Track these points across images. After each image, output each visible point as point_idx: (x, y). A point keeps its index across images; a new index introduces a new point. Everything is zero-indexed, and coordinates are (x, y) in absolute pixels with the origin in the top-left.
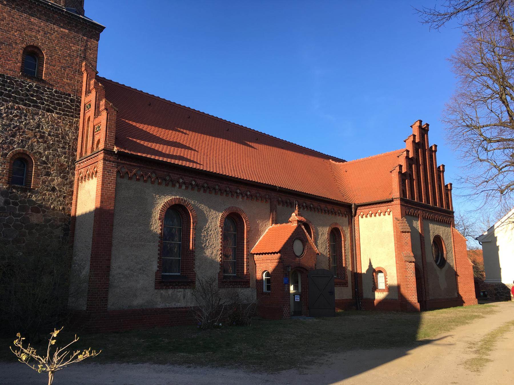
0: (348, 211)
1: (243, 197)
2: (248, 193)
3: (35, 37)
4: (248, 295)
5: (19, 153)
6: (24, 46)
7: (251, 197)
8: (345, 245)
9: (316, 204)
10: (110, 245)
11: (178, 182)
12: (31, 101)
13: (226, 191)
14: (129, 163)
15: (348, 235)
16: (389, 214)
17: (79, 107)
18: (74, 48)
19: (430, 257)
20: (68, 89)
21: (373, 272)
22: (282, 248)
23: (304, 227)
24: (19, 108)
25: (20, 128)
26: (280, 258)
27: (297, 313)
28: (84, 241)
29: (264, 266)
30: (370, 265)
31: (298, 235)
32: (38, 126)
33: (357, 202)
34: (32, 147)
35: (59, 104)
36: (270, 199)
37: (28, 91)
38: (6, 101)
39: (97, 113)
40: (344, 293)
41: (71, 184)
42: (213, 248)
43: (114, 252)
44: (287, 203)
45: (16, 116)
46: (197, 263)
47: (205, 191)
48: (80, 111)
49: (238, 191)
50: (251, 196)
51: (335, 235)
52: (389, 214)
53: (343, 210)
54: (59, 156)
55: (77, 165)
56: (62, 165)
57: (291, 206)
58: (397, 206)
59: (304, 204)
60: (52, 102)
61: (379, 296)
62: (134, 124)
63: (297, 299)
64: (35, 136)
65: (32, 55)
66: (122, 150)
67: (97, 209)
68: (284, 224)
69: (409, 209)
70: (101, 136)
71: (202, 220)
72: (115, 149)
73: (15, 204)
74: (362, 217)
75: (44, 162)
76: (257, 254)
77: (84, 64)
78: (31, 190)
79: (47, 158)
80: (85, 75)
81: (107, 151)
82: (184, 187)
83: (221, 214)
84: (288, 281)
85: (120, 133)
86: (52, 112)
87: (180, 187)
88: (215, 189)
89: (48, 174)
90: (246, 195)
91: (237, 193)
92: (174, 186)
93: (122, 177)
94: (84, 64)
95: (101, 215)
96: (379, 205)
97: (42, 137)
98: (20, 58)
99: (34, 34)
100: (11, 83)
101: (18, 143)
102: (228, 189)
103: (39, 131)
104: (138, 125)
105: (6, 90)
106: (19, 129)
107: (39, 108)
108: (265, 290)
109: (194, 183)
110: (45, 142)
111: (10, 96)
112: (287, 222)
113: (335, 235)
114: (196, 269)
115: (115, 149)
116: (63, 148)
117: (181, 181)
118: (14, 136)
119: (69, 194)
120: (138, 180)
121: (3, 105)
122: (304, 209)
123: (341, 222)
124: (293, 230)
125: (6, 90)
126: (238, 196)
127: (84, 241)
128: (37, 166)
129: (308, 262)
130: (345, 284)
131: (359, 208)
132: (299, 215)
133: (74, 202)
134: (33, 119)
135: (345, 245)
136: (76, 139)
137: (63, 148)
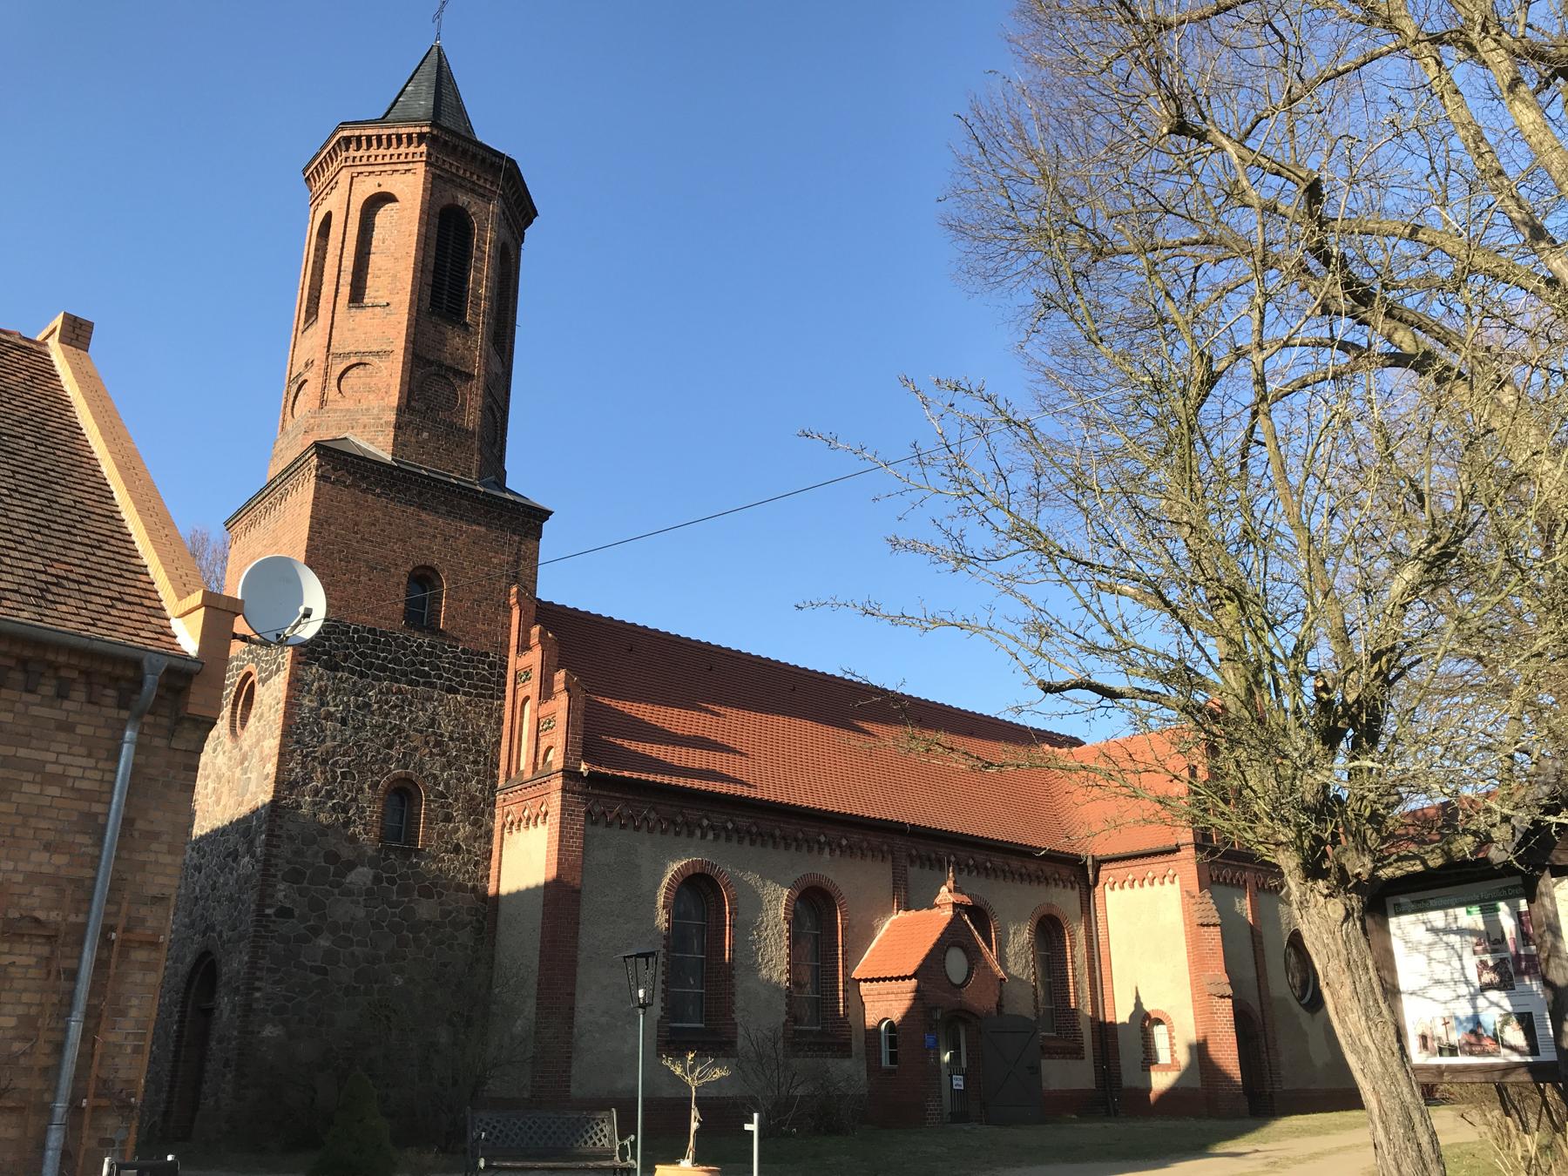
0: (1079, 874)
1: (832, 851)
2: (844, 842)
3: (429, 548)
4: (849, 1072)
5: (398, 779)
6: (409, 568)
7: (850, 851)
8: (1073, 957)
9: (998, 860)
10: (573, 962)
11: (700, 826)
12: (420, 673)
13: (796, 840)
14: (606, 795)
15: (1081, 932)
16: (1172, 882)
17: (503, 676)
18: (495, 561)
19: (1281, 985)
20: (484, 644)
21: (1144, 1021)
22: (920, 966)
23: (975, 914)
24: (400, 691)
25: (401, 730)
26: (917, 990)
27: (959, 1117)
28: (521, 948)
29: (885, 1005)
30: (1138, 1004)
31: (953, 937)
32: (433, 722)
33: (1101, 852)
34: (420, 767)
35: (468, 676)
36: (892, 853)
37: (416, 655)
38: (379, 679)
39: (546, 693)
40: (1068, 1075)
41: (489, 835)
42: (774, 960)
43: (581, 978)
44: (929, 859)
45: (396, 706)
46: (740, 1001)
47: (753, 843)
48: (505, 684)
49: (822, 839)
50: (850, 847)
51: (1050, 932)
52: (1172, 882)
53: (1065, 872)
54: (467, 780)
55: (500, 797)
56: (473, 798)
57: (939, 865)
58: (1187, 862)
59: (971, 862)
60: (457, 673)
61: (1161, 1081)
62: (606, 701)
63: (958, 1082)
64: (427, 743)
65: (424, 579)
66: (596, 768)
67: (547, 884)
68: (924, 911)
69: (1221, 870)
70: (557, 739)
71: (758, 905)
72: (584, 767)
73: (392, 881)
74: (1112, 889)
75: (442, 795)
76: (866, 980)
77: (514, 589)
78: (418, 853)
79: (447, 785)
80: (516, 613)
81: (569, 774)
82: (710, 836)
83: (786, 892)
84: (937, 1041)
85: (592, 732)
86: (456, 692)
87: (704, 836)
88: (772, 836)
89: (448, 818)
90: (840, 845)
91: (819, 842)
92: (691, 834)
93: (594, 823)
94: (514, 589)
95: (558, 895)
96: (1148, 860)
97: (438, 744)
98: (402, 592)
99: (426, 543)
100: (387, 643)
101: (398, 761)
102: (800, 835)
103: (434, 733)
104: (613, 703)
105: (378, 658)
106: (400, 732)
107: (432, 685)
108: (885, 1062)
109: (730, 826)
110: (443, 754)
111: (384, 669)
112: (931, 906)
113: (1050, 932)
114: (738, 1017)
115: (584, 767)
116: (476, 762)
117: (705, 822)
118: (390, 746)
119: (482, 853)
120: (623, 827)
121: (373, 687)
122: (970, 873)
123: (1064, 900)
124: (944, 925)
125: (378, 658)
126: (821, 850)
127: (521, 948)
128: (429, 802)
129: (980, 999)
130: (1076, 1053)
131: (1104, 867)
132: (956, 890)
133: (493, 872)
134: (424, 709)
135: (1073, 957)
136: (498, 743)
137: (476, 762)
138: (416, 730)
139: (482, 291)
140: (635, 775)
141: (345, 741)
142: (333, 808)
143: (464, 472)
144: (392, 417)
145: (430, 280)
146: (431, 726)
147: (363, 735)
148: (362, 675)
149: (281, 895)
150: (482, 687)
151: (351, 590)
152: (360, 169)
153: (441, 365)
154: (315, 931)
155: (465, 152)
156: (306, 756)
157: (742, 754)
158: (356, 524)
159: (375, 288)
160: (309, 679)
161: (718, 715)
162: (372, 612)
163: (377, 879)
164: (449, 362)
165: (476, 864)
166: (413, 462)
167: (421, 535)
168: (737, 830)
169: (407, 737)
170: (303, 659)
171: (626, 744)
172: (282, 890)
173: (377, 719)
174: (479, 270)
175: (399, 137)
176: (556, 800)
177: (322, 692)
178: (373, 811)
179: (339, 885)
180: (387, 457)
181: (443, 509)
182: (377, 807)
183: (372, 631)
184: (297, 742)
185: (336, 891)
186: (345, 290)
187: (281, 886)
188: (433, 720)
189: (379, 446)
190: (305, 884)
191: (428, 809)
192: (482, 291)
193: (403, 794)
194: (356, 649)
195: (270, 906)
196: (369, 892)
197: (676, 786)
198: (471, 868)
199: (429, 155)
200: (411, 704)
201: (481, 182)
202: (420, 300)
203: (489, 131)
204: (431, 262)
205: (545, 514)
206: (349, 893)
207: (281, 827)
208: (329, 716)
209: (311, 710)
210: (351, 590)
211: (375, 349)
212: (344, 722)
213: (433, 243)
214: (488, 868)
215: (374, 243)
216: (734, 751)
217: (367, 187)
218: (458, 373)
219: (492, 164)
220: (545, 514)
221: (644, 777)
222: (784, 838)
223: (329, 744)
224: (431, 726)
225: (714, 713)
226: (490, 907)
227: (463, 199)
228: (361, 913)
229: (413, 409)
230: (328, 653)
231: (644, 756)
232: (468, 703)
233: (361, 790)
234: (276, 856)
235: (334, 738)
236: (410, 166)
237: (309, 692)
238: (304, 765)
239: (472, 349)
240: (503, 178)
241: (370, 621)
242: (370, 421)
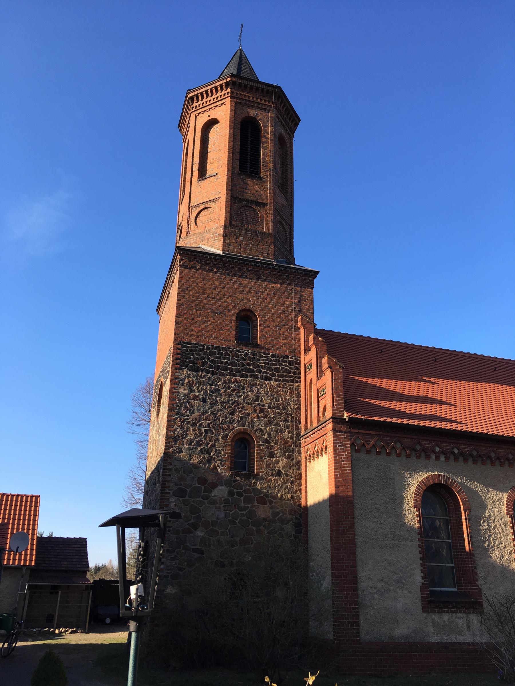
3: (247, 299)
5: (239, 433)
6: (237, 311)
11: (434, 451)
12: (247, 370)
14: (368, 433)
17: (298, 369)
18: (287, 303)
20: (285, 351)
25: (238, 404)
32: (257, 398)
35: (277, 370)
37: (244, 360)
38: (223, 375)
39: (320, 374)
41: (298, 464)
45: (234, 390)
46: (481, 573)
48: (300, 373)
54: (282, 431)
56: (286, 442)
60: (270, 369)
64: (255, 410)
65: (246, 318)
66: (354, 416)
70: (327, 401)
72: (346, 416)
73: (240, 495)
78: (255, 477)
79: (269, 435)
80: (302, 331)
81: (337, 420)
82: (443, 458)
83: (506, 496)
85: (349, 395)
88: (490, 457)
89: (272, 455)
92: (428, 457)
93: (358, 451)
97: (262, 411)
98: (233, 325)
100: (227, 354)
103: (259, 404)
105: (222, 363)
107: (256, 377)
109: (456, 451)
110: (265, 416)
111: (226, 369)
114: (480, 583)
116: (286, 421)
117: (437, 449)
118: (233, 413)
119: (297, 479)
120: (379, 453)
121: (220, 380)
125: (222, 363)
133: (303, 487)
136: (299, 408)
137: (286, 421)
138: (247, 403)
139: (268, 159)
140: (382, 419)
141: (206, 412)
142: (201, 451)
143: (266, 254)
144: (221, 231)
145: (238, 157)
146: (257, 400)
147: (216, 407)
148: (213, 373)
149: (172, 505)
150: (286, 376)
151: (203, 326)
152: (199, 111)
153: (247, 201)
154: (195, 527)
155: (251, 88)
156: (183, 422)
157: (451, 404)
158: (204, 290)
159: (210, 170)
160: (182, 377)
161: (434, 383)
162: (216, 337)
163: (231, 493)
164: (252, 198)
165: (292, 483)
166: (235, 253)
167: (242, 292)
168: (462, 454)
169: (243, 407)
170: (178, 366)
171: (378, 402)
173: (224, 398)
174: (265, 148)
176: (330, 437)
177: (190, 384)
178: (226, 453)
179: (207, 497)
180: (220, 252)
181: (254, 276)
182: (228, 450)
183: (217, 348)
184: (178, 414)
185: (206, 501)
186: (196, 173)
187: (172, 499)
188: (258, 397)
189: (215, 247)
190: (187, 498)
191: (259, 450)
192: (268, 159)
193: (243, 443)
194: (209, 359)
196: (226, 501)
197: (424, 427)
198: (289, 485)
199: (232, 92)
200: (243, 388)
201: (263, 102)
202: (234, 138)
203: (264, 75)
204: (238, 148)
205: (315, 274)
206: (214, 502)
207: (171, 464)
208: (195, 398)
209: (185, 395)
210: (203, 326)
212: (204, 401)
213: (238, 138)
214: (300, 485)
215: (209, 147)
216: (445, 403)
217: (203, 119)
218: (258, 204)
219: (268, 92)
220: (315, 274)
221: (388, 420)
222: (498, 458)
223: (196, 414)
224: (257, 400)
225: (429, 382)
226: (302, 514)
227: (252, 113)
228: (222, 515)
229: (234, 225)
230: (193, 362)
231: (384, 408)
232: (278, 386)
233: (217, 440)
234: (168, 481)
235: (199, 410)
236: (224, 101)
237: (183, 384)
238: (182, 427)
239: (264, 189)
240: (276, 96)
241: (216, 342)
242: (209, 237)
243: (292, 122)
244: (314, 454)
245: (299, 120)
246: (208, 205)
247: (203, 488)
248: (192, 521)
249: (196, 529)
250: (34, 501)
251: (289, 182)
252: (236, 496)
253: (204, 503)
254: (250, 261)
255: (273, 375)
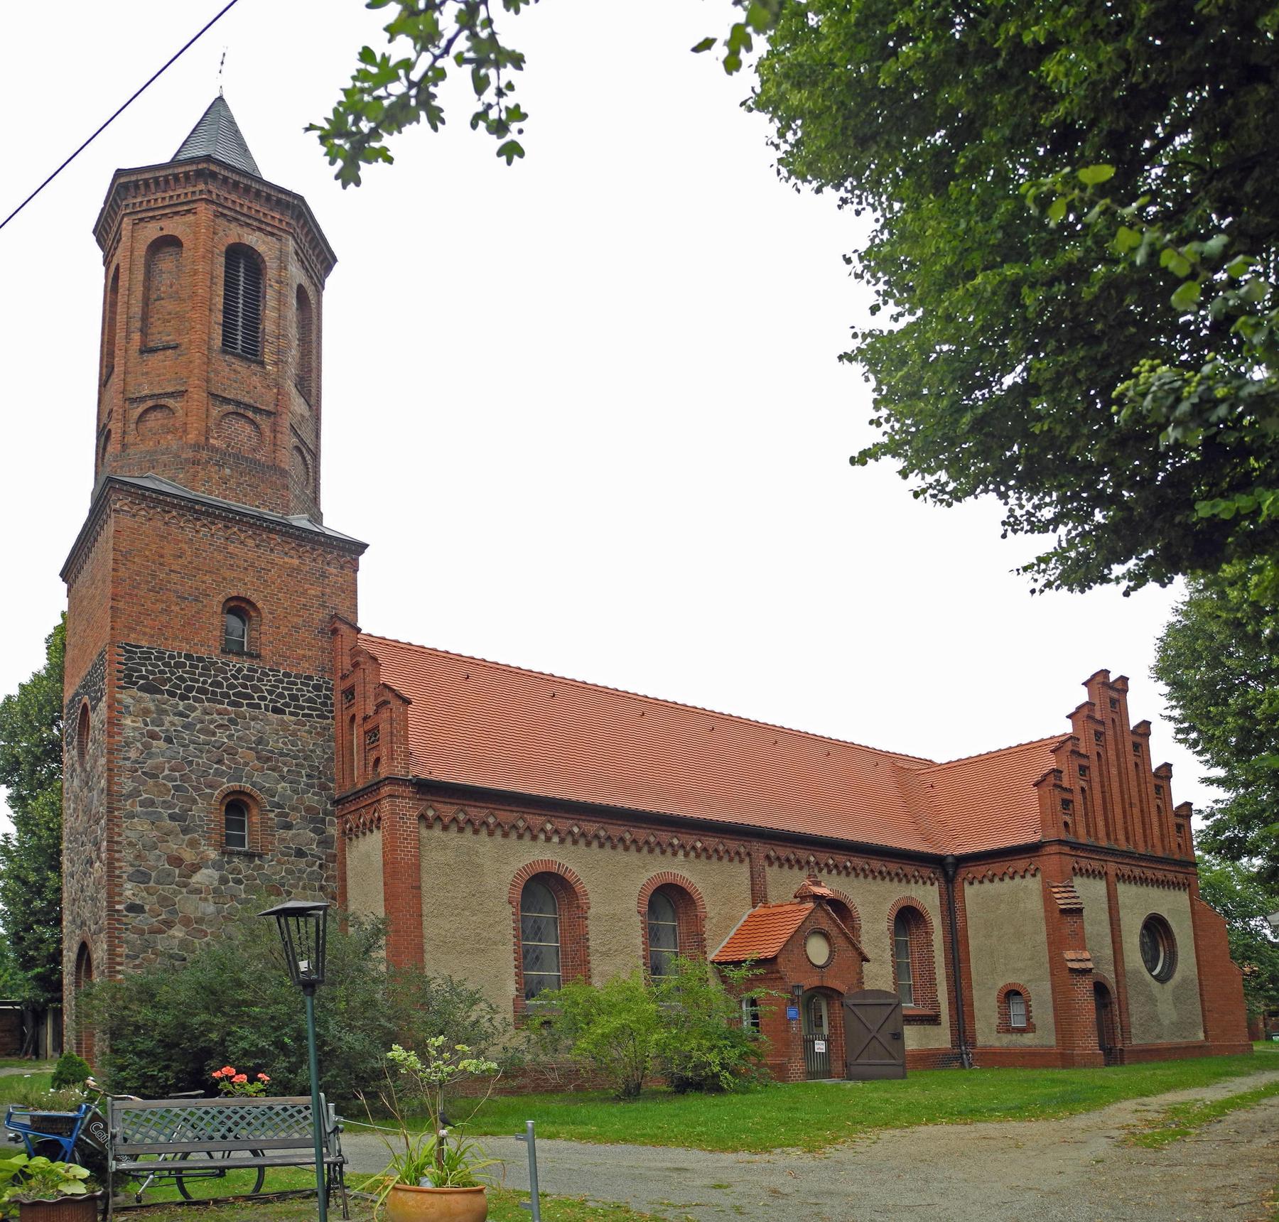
82: (556, 839)
87: (548, 839)
107: (258, 707)
109: (576, 830)
126: (675, 854)
154: (169, 924)
162: (187, 640)
163: (224, 880)
168: (583, 835)
172: (129, 890)
175: (176, 177)
185: (184, 890)
190: (152, 884)
195: (119, 903)
196: (215, 891)
205: (361, 547)
211: (170, 390)
220: (361, 547)
227: (253, 239)
234: (118, 860)
236: (192, 206)
243: (303, 227)
244: (358, 827)
245: (335, 260)
246: (162, 402)
247: (177, 871)
248: (163, 917)
249: (170, 927)
250: (1164, 585)
251: (314, 376)
252: (231, 884)
253: (181, 893)
254: (245, 515)
255: (287, 705)
